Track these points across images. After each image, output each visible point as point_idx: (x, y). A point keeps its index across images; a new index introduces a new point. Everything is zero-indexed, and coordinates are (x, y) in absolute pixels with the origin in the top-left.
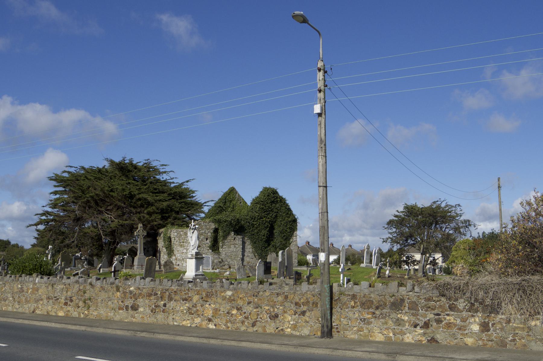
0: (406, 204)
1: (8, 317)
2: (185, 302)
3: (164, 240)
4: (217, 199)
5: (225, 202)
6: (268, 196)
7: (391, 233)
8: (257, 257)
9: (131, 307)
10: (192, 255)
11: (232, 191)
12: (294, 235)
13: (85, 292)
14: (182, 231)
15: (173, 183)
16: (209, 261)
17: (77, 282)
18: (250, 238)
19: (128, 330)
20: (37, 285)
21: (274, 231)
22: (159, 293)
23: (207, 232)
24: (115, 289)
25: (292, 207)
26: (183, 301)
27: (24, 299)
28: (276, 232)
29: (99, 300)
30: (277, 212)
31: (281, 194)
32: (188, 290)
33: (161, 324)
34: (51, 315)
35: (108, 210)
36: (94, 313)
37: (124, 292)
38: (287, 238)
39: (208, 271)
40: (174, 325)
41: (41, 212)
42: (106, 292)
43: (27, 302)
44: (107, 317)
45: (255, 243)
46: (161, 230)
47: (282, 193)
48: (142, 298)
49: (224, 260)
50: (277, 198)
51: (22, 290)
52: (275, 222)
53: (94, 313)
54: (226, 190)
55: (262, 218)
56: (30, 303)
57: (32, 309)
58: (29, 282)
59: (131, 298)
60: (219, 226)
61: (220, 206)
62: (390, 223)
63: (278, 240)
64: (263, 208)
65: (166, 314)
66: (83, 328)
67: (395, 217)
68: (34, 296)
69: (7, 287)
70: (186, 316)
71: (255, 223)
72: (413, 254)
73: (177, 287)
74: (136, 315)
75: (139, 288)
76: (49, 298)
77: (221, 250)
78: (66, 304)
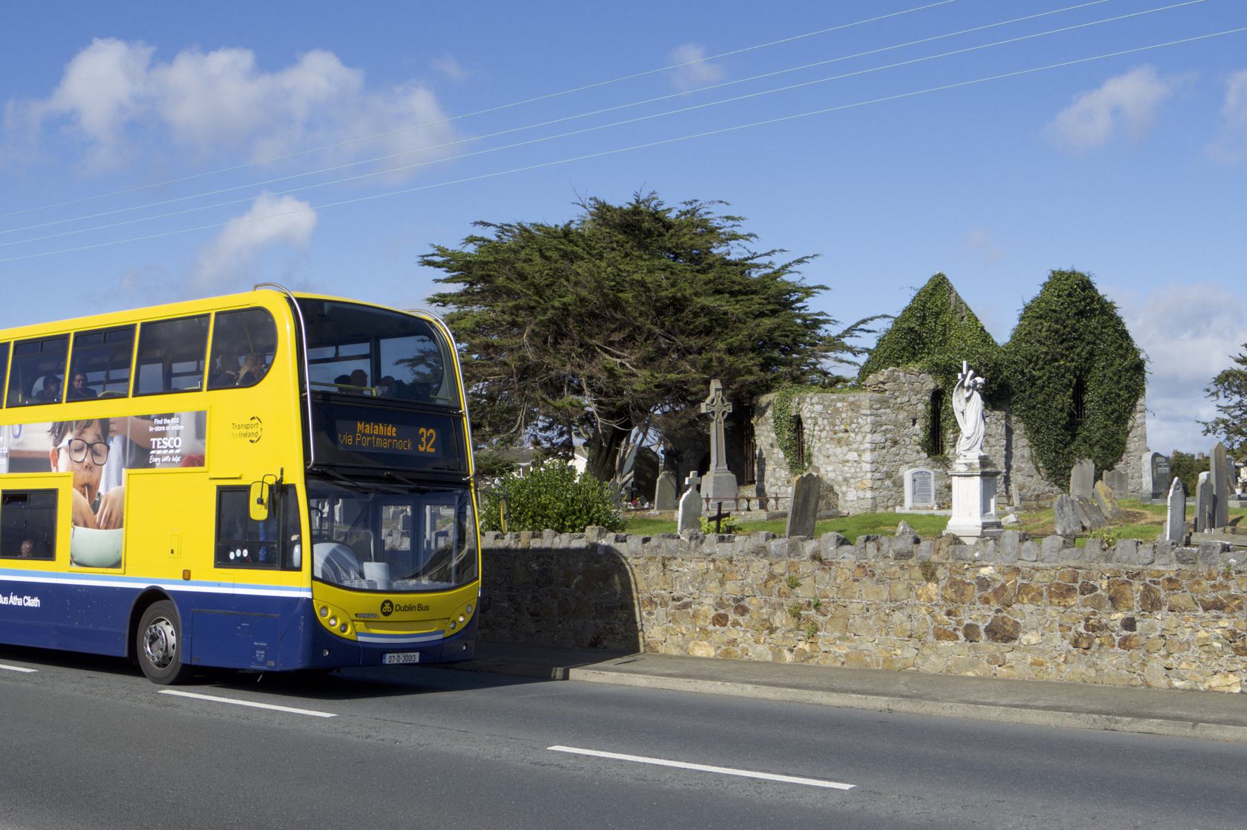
2: (1214, 613)
3: (778, 430)
4: (897, 313)
5: (924, 317)
6: (1070, 295)
9: (988, 630)
10: (969, 465)
11: (939, 285)
12: (1139, 408)
13: (794, 584)
14: (843, 400)
15: (758, 266)
16: (928, 485)
17: (761, 551)
18: (1025, 419)
19: (1077, 711)
21: (1086, 398)
22: (1105, 584)
23: (914, 400)
24: (917, 573)
25: (1131, 326)
26: (1206, 609)
29: (855, 607)
30: (1094, 343)
31: (1101, 293)
32: (1227, 575)
33: (1120, 684)
34: (664, 656)
35: (611, 344)
37: (953, 583)
38: (1119, 417)
40: (1172, 688)
42: (880, 581)
45: (1038, 431)
46: (764, 399)
47: (1104, 288)
48: (1032, 600)
52: (1088, 371)
54: (921, 281)
55: (1056, 360)
59: (986, 601)
61: (911, 330)
63: (1095, 423)
64: (1057, 331)
65: (1139, 654)
67: (1238, 361)
70: (1222, 661)
73: (1175, 566)
74: (1008, 656)
75: (1017, 570)
78: (720, 620)
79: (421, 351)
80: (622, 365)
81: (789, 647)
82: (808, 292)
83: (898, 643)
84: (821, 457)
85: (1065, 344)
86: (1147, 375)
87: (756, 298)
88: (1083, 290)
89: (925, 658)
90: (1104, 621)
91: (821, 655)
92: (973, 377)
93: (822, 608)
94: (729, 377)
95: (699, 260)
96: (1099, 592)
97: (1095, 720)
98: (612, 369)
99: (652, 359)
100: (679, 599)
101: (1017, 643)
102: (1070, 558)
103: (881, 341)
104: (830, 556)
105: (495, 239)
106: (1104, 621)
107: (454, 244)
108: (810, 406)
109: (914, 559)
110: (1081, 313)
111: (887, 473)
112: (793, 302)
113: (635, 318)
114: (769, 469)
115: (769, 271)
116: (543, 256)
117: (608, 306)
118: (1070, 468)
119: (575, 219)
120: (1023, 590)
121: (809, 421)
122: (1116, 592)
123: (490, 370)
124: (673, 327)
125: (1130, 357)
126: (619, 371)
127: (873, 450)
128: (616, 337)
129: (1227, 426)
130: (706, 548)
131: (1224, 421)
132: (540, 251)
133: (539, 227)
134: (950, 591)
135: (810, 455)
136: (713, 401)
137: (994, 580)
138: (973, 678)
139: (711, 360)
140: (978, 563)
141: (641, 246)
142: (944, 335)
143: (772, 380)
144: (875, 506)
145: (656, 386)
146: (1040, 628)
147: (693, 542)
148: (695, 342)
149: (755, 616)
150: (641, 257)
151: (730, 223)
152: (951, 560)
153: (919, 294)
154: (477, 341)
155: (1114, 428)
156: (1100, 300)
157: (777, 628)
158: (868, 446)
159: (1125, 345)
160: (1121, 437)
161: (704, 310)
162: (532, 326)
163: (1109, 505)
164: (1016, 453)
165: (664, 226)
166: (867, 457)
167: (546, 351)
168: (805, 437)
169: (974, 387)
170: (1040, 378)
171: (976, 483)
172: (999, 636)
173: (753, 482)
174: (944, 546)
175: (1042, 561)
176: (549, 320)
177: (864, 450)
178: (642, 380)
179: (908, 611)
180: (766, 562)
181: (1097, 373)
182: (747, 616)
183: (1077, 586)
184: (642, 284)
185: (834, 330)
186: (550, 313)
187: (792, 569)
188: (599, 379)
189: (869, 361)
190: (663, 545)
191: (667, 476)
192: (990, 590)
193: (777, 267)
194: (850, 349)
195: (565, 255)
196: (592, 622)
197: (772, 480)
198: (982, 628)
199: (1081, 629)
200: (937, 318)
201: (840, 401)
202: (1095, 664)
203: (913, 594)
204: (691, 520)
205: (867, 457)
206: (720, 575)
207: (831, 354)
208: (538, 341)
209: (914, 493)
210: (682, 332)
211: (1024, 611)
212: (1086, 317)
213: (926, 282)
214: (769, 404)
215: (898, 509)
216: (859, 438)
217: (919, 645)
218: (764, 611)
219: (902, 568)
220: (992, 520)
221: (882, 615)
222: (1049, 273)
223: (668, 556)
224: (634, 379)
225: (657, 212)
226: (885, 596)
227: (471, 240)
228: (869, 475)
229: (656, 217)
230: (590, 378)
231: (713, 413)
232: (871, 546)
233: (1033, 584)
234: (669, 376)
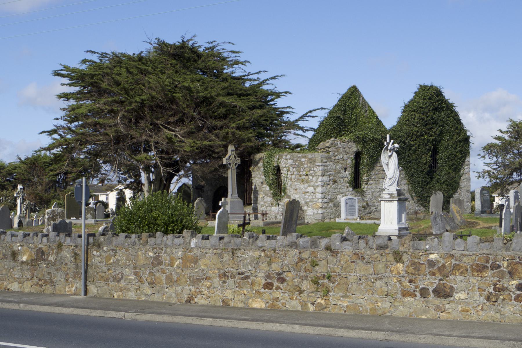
0: (511, 120)
1: (160, 314)
5: (345, 111)
6: (430, 99)
7: (488, 165)
9: (434, 291)
10: (391, 195)
11: (353, 93)
12: (466, 163)
13: (314, 264)
14: (305, 157)
15: (251, 80)
16: (354, 206)
17: (293, 245)
20: (195, 251)
21: (438, 157)
22: (505, 264)
24: (391, 258)
27: (163, 277)
28: (441, 157)
29: (352, 278)
31: (446, 98)
34: (234, 308)
35: (169, 123)
36: (339, 303)
37: (413, 264)
38: (456, 168)
39: (354, 222)
41: (52, 128)
42: (368, 263)
43: (170, 280)
44: (373, 309)
45: (412, 176)
46: (258, 156)
47: (449, 95)
48: (461, 274)
51: (157, 261)
52: (440, 142)
53: (339, 303)
54: (344, 90)
55: (423, 135)
56: (178, 285)
57: (185, 297)
58: (173, 246)
59: (434, 274)
60: (364, 147)
61: (338, 117)
63: (443, 172)
64: (423, 119)
66: (324, 331)
68: (188, 271)
69: (121, 255)
74: (447, 306)
75: (452, 256)
76: (225, 275)
78: (268, 286)
79: (56, 126)
80: (176, 136)
81: (314, 302)
82: (278, 95)
83: (379, 299)
84: (292, 190)
85: (428, 127)
86: (471, 144)
87: (252, 98)
88: (437, 96)
89: (396, 308)
90: (505, 286)
91: (331, 307)
92: (393, 143)
93: (332, 279)
94: (238, 142)
95: (218, 75)
96: (502, 268)
97: (514, 345)
98: (171, 138)
99: (193, 133)
100: (242, 274)
101: (452, 299)
102: (485, 249)
103: (321, 124)
104: (337, 248)
105: (98, 61)
106: (505, 286)
107: (75, 64)
108: (285, 161)
109: (389, 249)
110: (436, 109)
111: (330, 199)
112: (269, 101)
113: (184, 109)
114: (260, 196)
115: (256, 83)
116: (129, 72)
117: (168, 102)
118: (430, 197)
119: (144, 50)
120: (456, 267)
121: (285, 169)
122: (513, 269)
123: (98, 138)
124: (206, 114)
126: (175, 140)
127: (323, 186)
128: (172, 119)
129: (489, 174)
130: (259, 243)
131: (488, 171)
132: (127, 68)
133: (124, 55)
134: (411, 268)
135: (285, 189)
136: (230, 157)
137: (438, 262)
138: (428, 320)
139: (227, 133)
140: (428, 252)
141: (185, 67)
142: (356, 121)
143: (261, 145)
144: (324, 218)
145: (197, 149)
146: (466, 290)
147: (251, 240)
148: (219, 123)
149: (290, 284)
150: (185, 73)
151: (234, 55)
152: (411, 250)
153: (342, 97)
154: (89, 121)
155: (453, 174)
156: (446, 101)
157: (304, 291)
158: (320, 183)
159: (459, 127)
161: (222, 104)
162: (123, 112)
163: (459, 218)
165: (197, 56)
166: (319, 190)
167: (130, 127)
168: (282, 178)
169: (393, 149)
170: (414, 145)
171: (395, 205)
172: (441, 294)
173: (251, 204)
174: (407, 242)
175: (467, 250)
176: (133, 109)
177: (318, 186)
178: (188, 145)
179: (386, 280)
180: (297, 251)
181: (444, 143)
182: (285, 284)
183: (489, 265)
184: (188, 89)
185: (292, 118)
186: (134, 106)
187: (313, 255)
188: (162, 144)
189: (314, 135)
190: (232, 241)
191: (200, 201)
192: (435, 268)
193: (261, 81)
194: (302, 129)
195: (141, 72)
196: (187, 287)
197: (262, 203)
198: (431, 290)
199: (491, 290)
200: (352, 111)
201: (303, 158)
202: (500, 311)
203: (388, 270)
204: (223, 227)
205: (319, 190)
206: (268, 259)
207: (292, 131)
208: (126, 121)
209: (347, 211)
210: (211, 118)
211: (456, 280)
213: (346, 91)
214: (260, 159)
215: (337, 220)
216: (315, 179)
217: (392, 300)
218: (296, 280)
219: (381, 255)
220: (403, 226)
221: (369, 283)
222: (418, 86)
223: (236, 248)
224: (183, 144)
225: (193, 48)
226: (371, 271)
227: (84, 61)
228: (320, 200)
229: (193, 50)
230: (157, 143)
231: (230, 164)
232: (362, 242)
233: (462, 264)
234: (204, 143)
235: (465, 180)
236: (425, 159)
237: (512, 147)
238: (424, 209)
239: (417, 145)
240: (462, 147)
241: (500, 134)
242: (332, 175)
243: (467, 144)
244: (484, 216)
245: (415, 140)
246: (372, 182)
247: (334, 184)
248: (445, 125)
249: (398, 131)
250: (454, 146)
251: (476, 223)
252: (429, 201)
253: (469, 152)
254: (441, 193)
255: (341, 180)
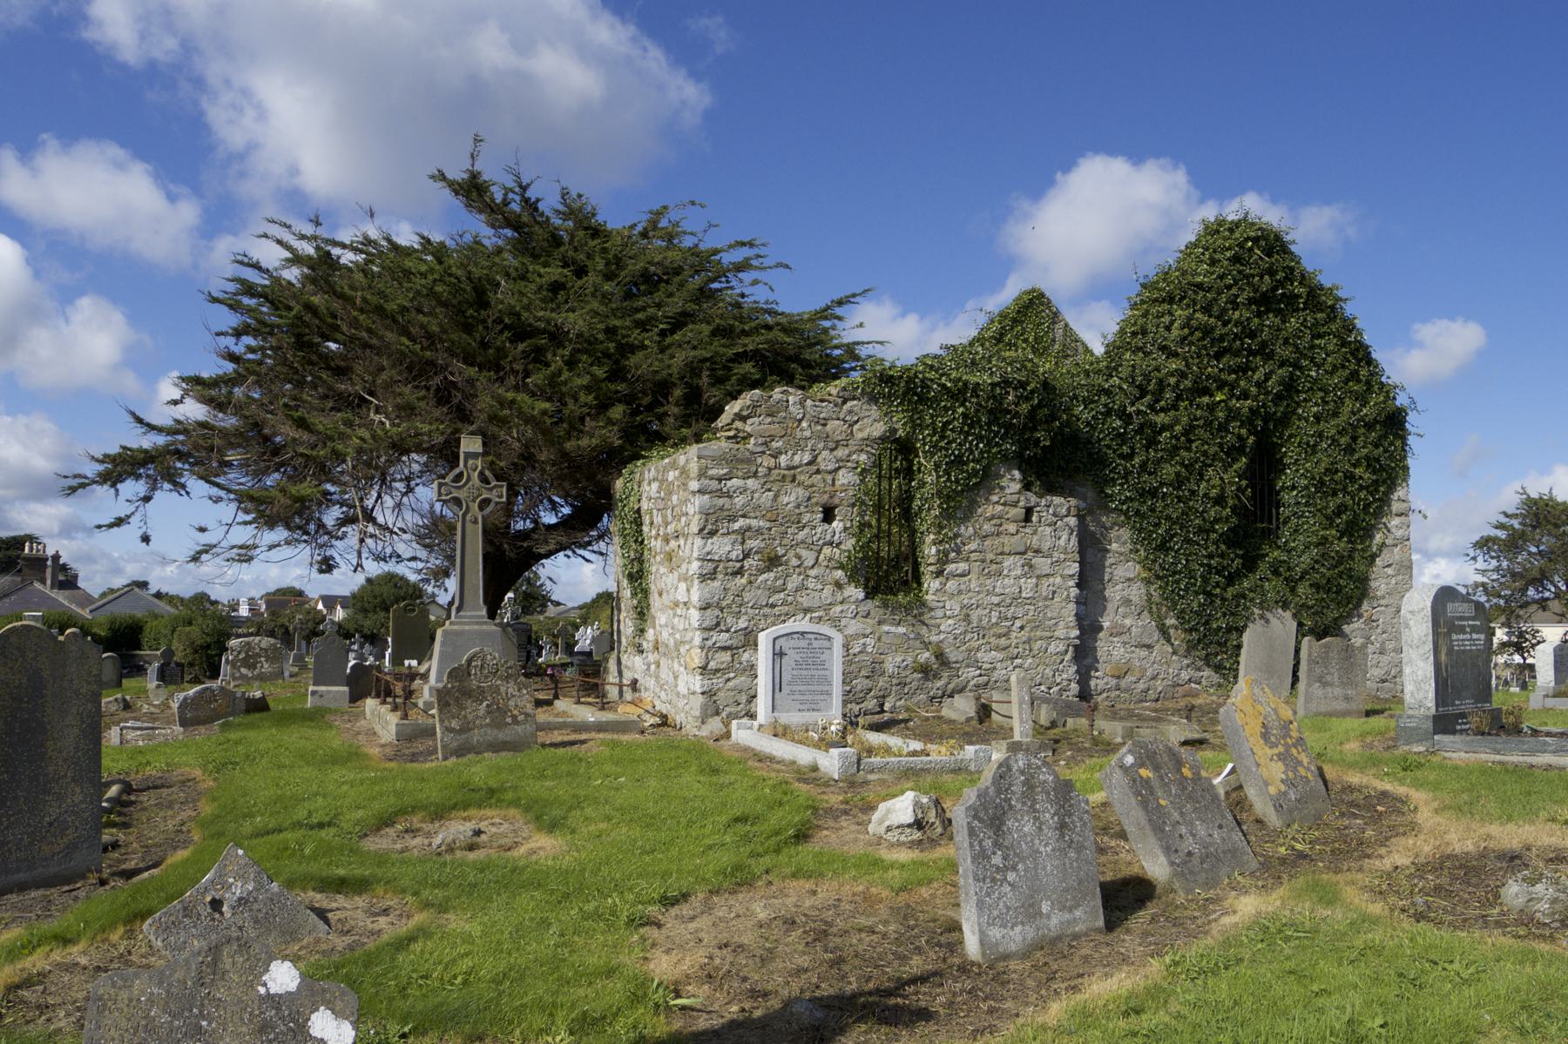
6: (1236, 259)
8: (1178, 637)
12: (1396, 507)
23: (826, 460)
28: (1293, 481)
30: (1296, 366)
45: (1163, 547)
49: (953, 655)
50: (1289, 278)
52: (1284, 421)
55: (1206, 391)
60: (915, 424)
62: (1484, 544)
63: (1301, 535)
64: (1207, 331)
71: (1161, 419)
72: (1537, 626)
77: (931, 584)
86: (1411, 440)
118: (1240, 631)
125: (1374, 399)
127: (705, 578)
131: (1483, 585)
159: (1363, 372)
160: (1359, 566)
163: (1277, 771)
164: (1114, 593)
170: (1164, 428)
181: (1303, 429)
212: (1278, 312)
235: (1389, 571)
236: (1217, 481)
237: (1525, 541)
238: (1216, 678)
239: (1178, 428)
240: (1376, 446)
241: (1504, 520)
242: (759, 531)
243: (1397, 436)
244: (1458, 751)
245: (1175, 407)
246: (963, 566)
247: (769, 570)
248: (1304, 363)
249: (1098, 372)
250: (1344, 440)
251: (1397, 804)
252: (1239, 647)
253: (1406, 469)
254: (1288, 615)
255: (804, 553)
